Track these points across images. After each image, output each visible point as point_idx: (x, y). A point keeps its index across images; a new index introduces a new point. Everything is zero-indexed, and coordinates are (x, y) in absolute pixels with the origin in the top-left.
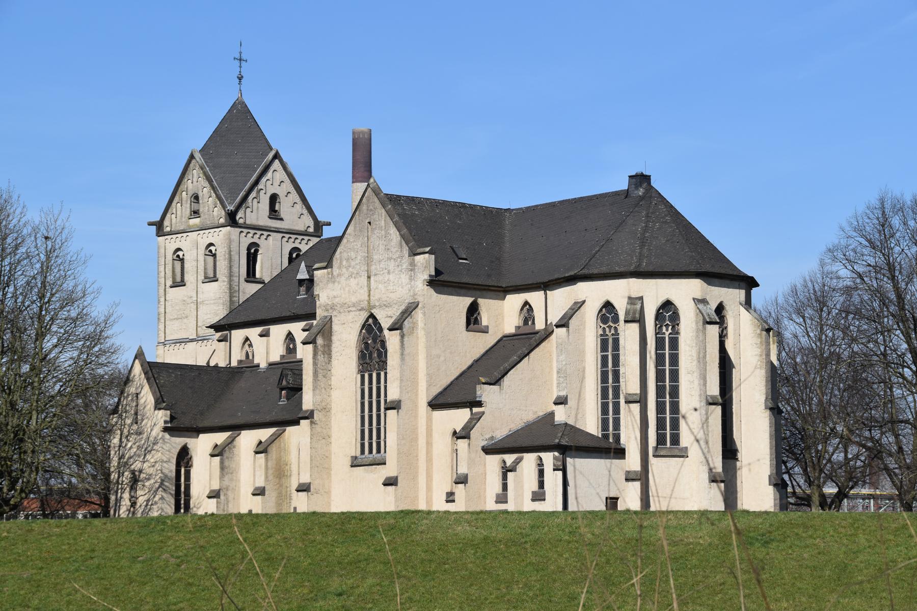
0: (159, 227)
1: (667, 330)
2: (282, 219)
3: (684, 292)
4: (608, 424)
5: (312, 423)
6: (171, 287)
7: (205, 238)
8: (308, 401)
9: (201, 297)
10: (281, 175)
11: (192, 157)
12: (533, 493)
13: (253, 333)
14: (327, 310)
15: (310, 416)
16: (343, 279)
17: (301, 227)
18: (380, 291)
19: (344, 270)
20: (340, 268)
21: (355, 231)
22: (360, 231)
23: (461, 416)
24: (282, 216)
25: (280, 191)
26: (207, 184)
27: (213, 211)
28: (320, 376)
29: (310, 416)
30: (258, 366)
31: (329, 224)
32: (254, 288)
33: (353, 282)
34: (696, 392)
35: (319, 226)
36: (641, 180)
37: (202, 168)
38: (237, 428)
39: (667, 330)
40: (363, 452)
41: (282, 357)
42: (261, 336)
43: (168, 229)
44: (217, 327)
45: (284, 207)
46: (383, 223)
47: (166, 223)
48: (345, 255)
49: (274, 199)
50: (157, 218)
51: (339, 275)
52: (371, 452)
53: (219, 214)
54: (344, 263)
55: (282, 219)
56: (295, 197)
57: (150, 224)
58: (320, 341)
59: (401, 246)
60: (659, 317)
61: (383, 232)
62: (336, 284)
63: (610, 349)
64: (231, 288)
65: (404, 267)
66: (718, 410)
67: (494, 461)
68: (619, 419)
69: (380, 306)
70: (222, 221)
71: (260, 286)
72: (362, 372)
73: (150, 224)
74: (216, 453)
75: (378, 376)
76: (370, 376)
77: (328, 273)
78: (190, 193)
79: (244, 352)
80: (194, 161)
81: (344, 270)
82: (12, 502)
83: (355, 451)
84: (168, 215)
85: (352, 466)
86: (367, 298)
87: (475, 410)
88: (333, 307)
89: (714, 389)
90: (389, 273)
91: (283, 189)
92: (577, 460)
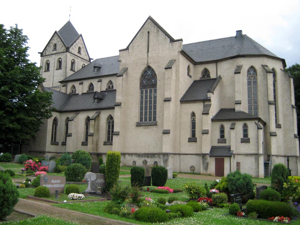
0: (42, 54)
1: (252, 78)
2: (81, 54)
4: (112, 127)
6: (44, 72)
7: (57, 57)
9: (55, 74)
12: (218, 140)
13: (76, 84)
15: (119, 105)
17: (85, 58)
23: (198, 108)
24: (81, 54)
25: (81, 46)
27: (60, 48)
29: (119, 105)
30: (78, 94)
32: (72, 73)
35: (90, 59)
36: (239, 32)
38: (77, 111)
40: (141, 119)
41: (87, 91)
43: (45, 55)
44: (61, 82)
45: (82, 51)
46: (156, 31)
47: (44, 53)
49: (79, 48)
50: (41, 51)
52: (146, 120)
55: (81, 54)
57: (39, 53)
60: (248, 71)
67: (218, 125)
70: (65, 51)
71: (74, 72)
72: (141, 89)
73: (39, 53)
76: (146, 92)
78: (54, 44)
79: (72, 90)
82: (191, 192)
83: (138, 120)
85: (137, 126)
87: (206, 103)
89: (271, 99)
92: (47, 145)
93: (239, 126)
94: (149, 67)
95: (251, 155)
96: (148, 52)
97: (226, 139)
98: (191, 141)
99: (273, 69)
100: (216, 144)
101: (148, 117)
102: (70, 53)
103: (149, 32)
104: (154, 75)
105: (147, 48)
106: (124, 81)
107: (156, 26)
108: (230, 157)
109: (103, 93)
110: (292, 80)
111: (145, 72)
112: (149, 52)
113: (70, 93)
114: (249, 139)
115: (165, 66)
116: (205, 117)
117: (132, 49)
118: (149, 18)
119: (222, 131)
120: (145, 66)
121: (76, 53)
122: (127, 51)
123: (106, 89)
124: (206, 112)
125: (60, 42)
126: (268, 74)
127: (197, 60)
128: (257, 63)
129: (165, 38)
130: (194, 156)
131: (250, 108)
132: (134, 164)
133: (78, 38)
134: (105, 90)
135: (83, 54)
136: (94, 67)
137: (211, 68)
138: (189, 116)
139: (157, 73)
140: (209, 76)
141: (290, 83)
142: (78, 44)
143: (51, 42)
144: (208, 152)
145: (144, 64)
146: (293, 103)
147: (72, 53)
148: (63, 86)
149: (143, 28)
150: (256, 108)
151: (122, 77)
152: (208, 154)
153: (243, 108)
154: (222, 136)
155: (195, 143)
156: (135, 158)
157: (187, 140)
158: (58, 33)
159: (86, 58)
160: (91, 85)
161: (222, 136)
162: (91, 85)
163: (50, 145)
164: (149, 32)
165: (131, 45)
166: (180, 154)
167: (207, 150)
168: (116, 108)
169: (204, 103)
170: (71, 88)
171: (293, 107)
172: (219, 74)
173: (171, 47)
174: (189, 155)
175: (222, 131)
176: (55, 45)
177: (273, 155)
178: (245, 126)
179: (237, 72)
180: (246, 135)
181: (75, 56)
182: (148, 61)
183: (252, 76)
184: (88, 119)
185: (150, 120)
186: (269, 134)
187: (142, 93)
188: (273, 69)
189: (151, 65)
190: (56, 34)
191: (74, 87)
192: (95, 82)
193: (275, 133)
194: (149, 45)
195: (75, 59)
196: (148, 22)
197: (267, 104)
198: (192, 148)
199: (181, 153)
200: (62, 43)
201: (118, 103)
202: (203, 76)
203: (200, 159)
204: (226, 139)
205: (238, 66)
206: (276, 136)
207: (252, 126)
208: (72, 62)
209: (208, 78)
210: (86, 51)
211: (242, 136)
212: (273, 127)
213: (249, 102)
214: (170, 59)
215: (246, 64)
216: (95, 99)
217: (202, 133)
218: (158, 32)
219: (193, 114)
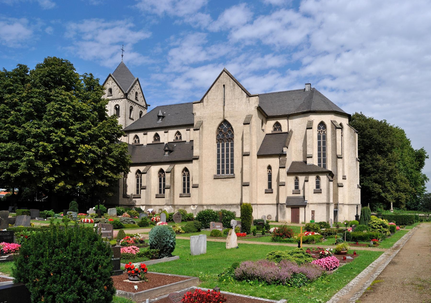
8: (196, 152)
10: (138, 86)
11: (110, 75)
17: (142, 105)
23: (275, 162)
29: (197, 159)
30: (143, 145)
31: (150, 106)
32: (132, 122)
34: (205, 165)
40: (218, 172)
41: (153, 142)
45: (140, 96)
46: (232, 85)
49: (137, 93)
52: (223, 172)
53: (121, 95)
56: (141, 95)
64: (125, 120)
67: (292, 179)
70: (122, 97)
75: (227, 145)
78: (108, 88)
91: (139, 91)
93: (312, 179)
94: (225, 121)
95: (323, 204)
99: (341, 124)
100: (291, 195)
101: (225, 168)
103: (224, 86)
105: (222, 102)
107: (231, 80)
108: (305, 206)
110: (357, 135)
111: (221, 125)
112: (225, 106)
113: (133, 143)
114: (321, 190)
115: (243, 121)
116: (281, 170)
117: (207, 102)
118: (224, 71)
119: (297, 183)
120: (222, 120)
121: (134, 100)
122: (202, 103)
123: (174, 140)
124: (283, 166)
125: (116, 87)
126: (337, 130)
127: (269, 114)
128: (327, 119)
129: (242, 92)
130: (271, 206)
131: (319, 161)
133: (135, 83)
134: (172, 141)
136: (158, 116)
137: (283, 122)
138: (266, 169)
139: (233, 127)
140: (280, 129)
141: (355, 137)
142: (135, 89)
144: (285, 202)
145: (220, 118)
146: (357, 157)
147: (130, 99)
149: (218, 80)
150: (325, 161)
151: (199, 131)
152: (285, 204)
153: (314, 161)
154: (297, 187)
157: (264, 191)
158: (112, 76)
159: (143, 104)
160: (157, 135)
161: (297, 187)
162: (157, 135)
164: (224, 86)
165: (206, 97)
166: (257, 204)
167: (283, 200)
168: (194, 161)
171: (357, 160)
172: (290, 128)
173: (248, 102)
174: (266, 205)
175: (297, 183)
176: (110, 90)
177: (340, 204)
178: (297, 178)
179: (309, 128)
180: (318, 186)
182: (224, 115)
183: (322, 131)
184: (161, 171)
185: (227, 172)
186: (336, 185)
187: (218, 146)
188: (341, 124)
189: (227, 119)
190: (110, 77)
191: (137, 137)
192: (161, 133)
193: (342, 184)
194: (224, 99)
196: (223, 75)
197: (335, 157)
198: (271, 199)
199: (258, 203)
201: (196, 156)
202: (275, 129)
205: (310, 121)
206: (342, 186)
207: (324, 179)
209: (280, 132)
211: (315, 188)
212: (340, 180)
213: (319, 155)
214: (247, 114)
215: (316, 119)
218: (234, 85)
219: (269, 167)
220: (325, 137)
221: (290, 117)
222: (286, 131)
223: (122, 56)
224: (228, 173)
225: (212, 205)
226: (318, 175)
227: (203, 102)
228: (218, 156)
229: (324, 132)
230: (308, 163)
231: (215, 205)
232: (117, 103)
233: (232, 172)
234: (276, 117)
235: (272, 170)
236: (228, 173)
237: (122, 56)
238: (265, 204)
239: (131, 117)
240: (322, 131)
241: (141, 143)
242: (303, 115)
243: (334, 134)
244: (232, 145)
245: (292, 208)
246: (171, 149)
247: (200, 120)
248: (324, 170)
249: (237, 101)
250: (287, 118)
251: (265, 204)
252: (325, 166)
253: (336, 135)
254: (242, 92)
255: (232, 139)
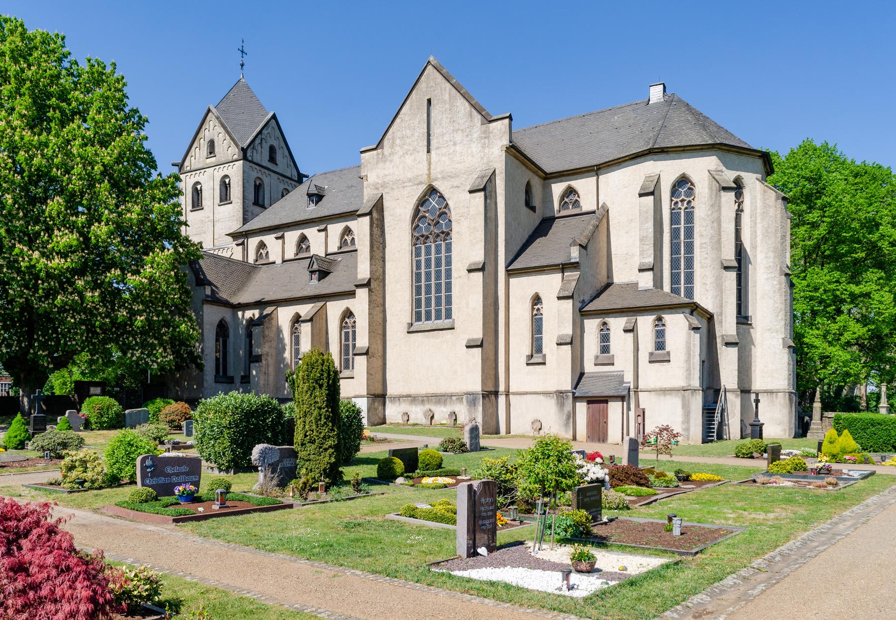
1: (683, 205)
3: (701, 169)
5: (370, 290)
11: (209, 111)
14: (377, 189)
16: (396, 158)
17: (289, 174)
18: (441, 161)
19: (398, 148)
20: (392, 147)
21: (410, 110)
22: (418, 109)
25: (275, 143)
26: (222, 130)
28: (375, 249)
30: (274, 263)
33: (409, 160)
37: (218, 118)
39: (683, 205)
42: (277, 238)
43: (188, 168)
45: (279, 157)
46: (447, 97)
47: (187, 163)
48: (399, 134)
49: (272, 149)
50: (180, 161)
51: (391, 154)
54: (398, 142)
58: (375, 215)
59: (471, 115)
60: (674, 192)
61: (447, 106)
62: (388, 163)
63: (443, 264)
65: (476, 135)
66: (733, 275)
68: (692, 274)
69: (443, 178)
70: (236, 157)
74: (567, 294)
75: (438, 251)
77: (378, 154)
78: (207, 140)
80: (210, 114)
81: (398, 148)
84: (188, 157)
86: (426, 172)
88: (384, 185)
89: (729, 254)
90: (455, 144)
93: (646, 323)
94: (432, 191)
96: (428, 151)
97: (613, 356)
98: (532, 361)
102: (250, 161)
103: (429, 101)
104: (444, 213)
106: (375, 230)
109: (331, 257)
111: (422, 202)
122: (379, 151)
130: (541, 397)
132: (406, 418)
135: (282, 164)
138: (528, 304)
140: (576, 204)
143: (201, 135)
145: (421, 183)
147: (255, 160)
148: (237, 245)
154: (605, 349)
155: (541, 366)
156: (404, 407)
159: (291, 172)
160: (303, 239)
162: (303, 239)
163: (214, 384)
164: (429, 101)
169: (563, 272)
170: (258, 251)
174: (529, 396)
176: (212, 144)
180: (660, 346)
181: (263, 170)
183: (682, 201)
187: (418, 254)
189: (436, 184)
191: (262, 245)
192: (311, 233)
195: (264, 178)
200: (228, 138)
203: (551, 404)
204: (613, 356)
208: (255, 185)
210: (287, 154)
215: (668, 170)
216: (312, 272)
217: (558, 344)
219: (537, 300)
220: (755, 232)
221: (601, 171)
222: (593, 207)
223: (242, 65)
224: (420, 320)
225: (403, 396)
226: (659, 313)
227: (383, 148)
228: (418, 275)
229: (689, 202)
230: (640, 285)
231: (408, 396)
232: (225, 172)
233: (449, 315)
234: (568, 175)
235: (544, 306)
236: (420, 320)
237: (242, 65)
238: (526, 393)
239: (260, 202)
240: (682, 201)
241: (271, 260)
242: (632, 162)
243: (716, 206)
244: (449, 249)
245: (589, 402)
246: (325, 267)
247: (376, 192)
248: (676, 300)
249: (458, 137)
250: (594, 173)
251: (526, 393)
252: (690, 292)
253: (720, 207)
254: (471, 115)
255: (448, 234)
